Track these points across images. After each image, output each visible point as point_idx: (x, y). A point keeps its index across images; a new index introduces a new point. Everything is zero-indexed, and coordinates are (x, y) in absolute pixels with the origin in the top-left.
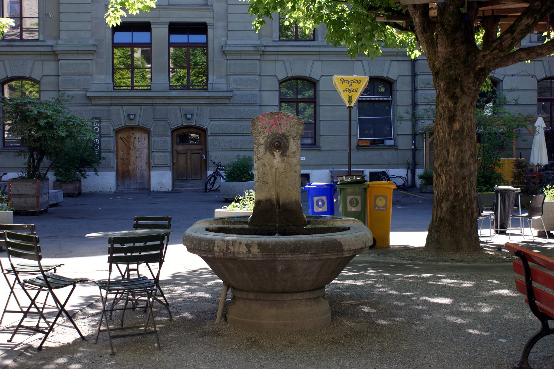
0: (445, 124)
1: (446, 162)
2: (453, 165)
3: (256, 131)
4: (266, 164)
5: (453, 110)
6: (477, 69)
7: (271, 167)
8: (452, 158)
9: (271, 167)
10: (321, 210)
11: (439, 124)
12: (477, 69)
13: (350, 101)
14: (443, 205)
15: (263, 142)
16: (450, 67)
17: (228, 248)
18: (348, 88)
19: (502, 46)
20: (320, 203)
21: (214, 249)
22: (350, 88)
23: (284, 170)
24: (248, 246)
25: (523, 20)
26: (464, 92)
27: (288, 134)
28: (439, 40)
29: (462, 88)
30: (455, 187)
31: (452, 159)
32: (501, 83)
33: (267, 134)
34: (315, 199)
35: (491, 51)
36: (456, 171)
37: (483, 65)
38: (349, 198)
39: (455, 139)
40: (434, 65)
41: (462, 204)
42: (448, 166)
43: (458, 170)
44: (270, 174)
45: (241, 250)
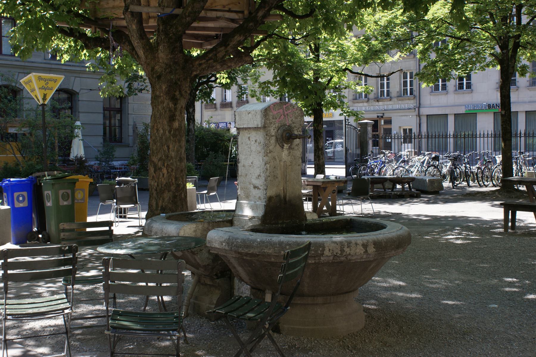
0: (165, 122)
1: (168, 157)
2: (174, 160)
3: (268, 122)
4: (276, 157)
5: (173, 110)
6: (192, 75)
7: (280, 161)
8: (173, 153)
9: (280, 161)
10: (21, 205)
11: (159, 122)
12: (192, 75)
13: (44, 99)
14: (165, 195)
15: (273, 134)
16: (171, 72)
17: (342, 251)
18: (45, 85)
19: (217, 57)
20: (21, 199)
21: (323, 254)
22: (46, 86)
23: (290, 164)
24: (365, 246)
25: (236, 37)
26: (182, 95)
27: (293, 125)
28: (161, 47)
29: (180, 92)
30: (176, 179)
31: (173, 154)
32: (21, 92)
33: (277, 125)
34: (16, 194)
35: (207, 61)
36: (177, 165)
37: (198, 72)
38: (61, 192)
39: (175, 136)
40: (153, 69)
41: (181, 193)
42: (170, 160)
43: (178, 164)
44: (279, 168)
45: (358, 251)
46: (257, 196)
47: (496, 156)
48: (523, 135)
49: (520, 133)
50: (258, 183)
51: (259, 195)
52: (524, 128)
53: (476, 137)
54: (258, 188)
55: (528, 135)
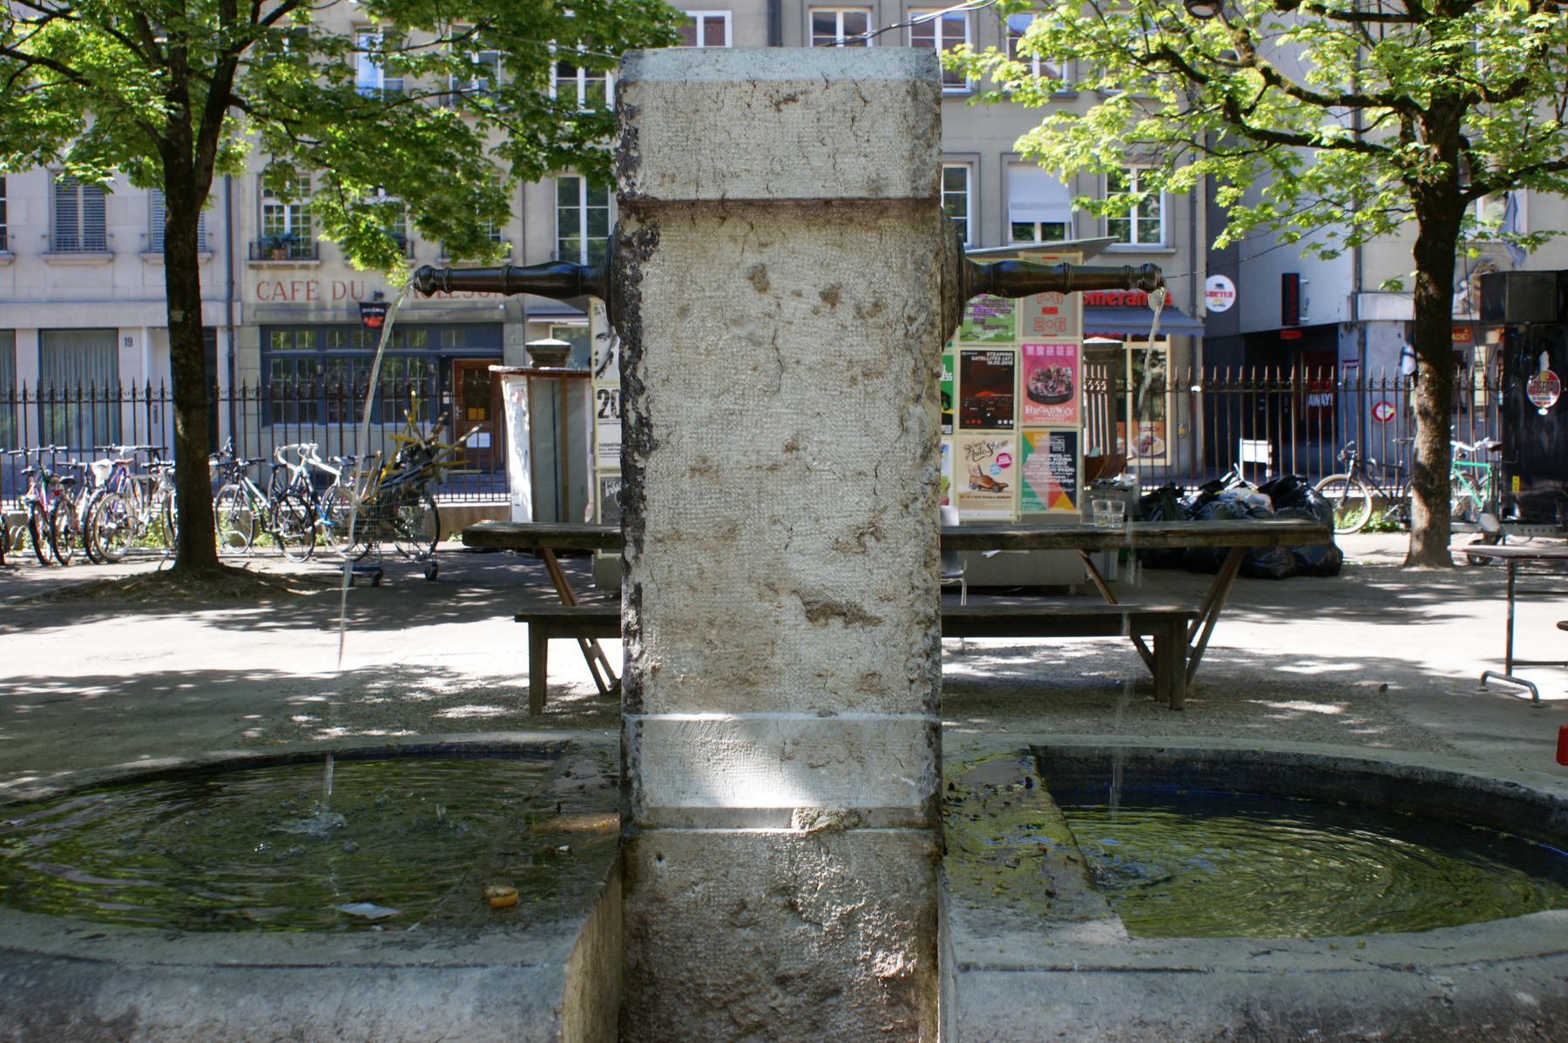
46: (849, 671)
47: (94, 465)
48: (34, 398)
49: (149, 390)
50: (846, 579)
51: (864, 663)
52: (36, 376)
53: (119, 401)
54: (852, 615)
55: (46, 399)
